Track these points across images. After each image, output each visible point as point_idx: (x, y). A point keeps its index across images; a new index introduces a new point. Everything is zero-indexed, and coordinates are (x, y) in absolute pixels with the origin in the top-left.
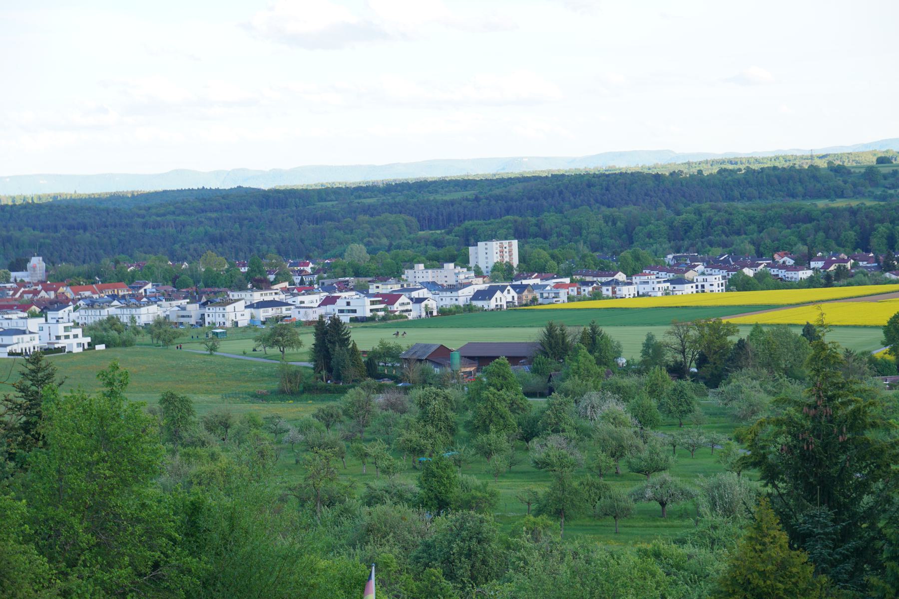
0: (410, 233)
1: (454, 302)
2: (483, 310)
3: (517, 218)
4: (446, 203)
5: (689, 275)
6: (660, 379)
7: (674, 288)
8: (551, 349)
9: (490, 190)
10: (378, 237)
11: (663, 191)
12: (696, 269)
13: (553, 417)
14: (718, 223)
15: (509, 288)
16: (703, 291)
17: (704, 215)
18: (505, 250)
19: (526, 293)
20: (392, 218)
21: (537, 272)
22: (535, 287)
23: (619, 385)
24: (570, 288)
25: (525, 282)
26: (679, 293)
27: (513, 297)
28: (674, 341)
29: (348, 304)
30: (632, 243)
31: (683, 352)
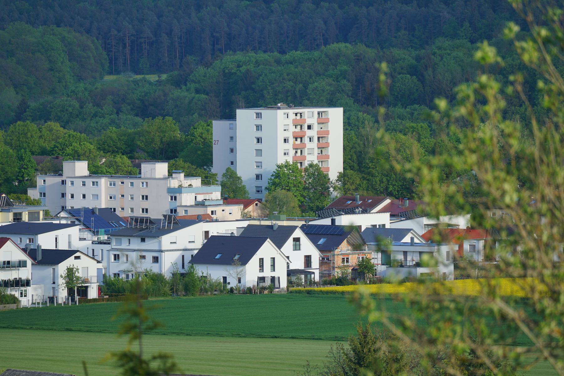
1: (147, 265)
15: (298, 233)
18: (309, 133)
19: (344, 247)
27: (308, 259)
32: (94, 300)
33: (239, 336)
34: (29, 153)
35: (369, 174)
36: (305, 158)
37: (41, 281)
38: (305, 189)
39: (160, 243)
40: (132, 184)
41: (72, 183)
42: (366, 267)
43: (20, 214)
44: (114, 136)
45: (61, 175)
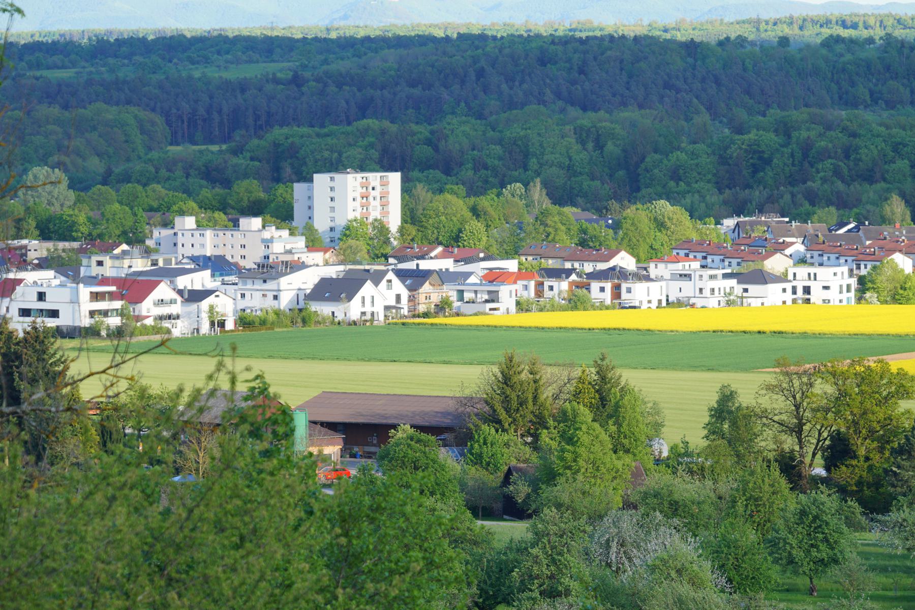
0: (150, 149)
1: (269, 303)
2: (333, 323)
3: (386, 124)
4: (227, 86)
5: (775, 264)
6: (766, 488)
7: (746, 290)
8: (507, 410)
9: (326, 62)
10: (78, 154)
11: (703, 80)
12: (788, 251)
13: (545, 562)
14: (824, 154)
15: (391, 275)
16: (808, 301)
17: (795, 134)
18: (373, 193)
19: (426, 287)
20: (111, 113)
21: (440, 243)
22: (444, 277)
23: (676, 497)
24: (521, 283)
25: (425, 265)
26: (756, 303)
27: (398, 298)
28: (779, 405)
29: (41, 296)
30: (638, 190)
31: (797, 430)
32: (232, 331)
33: (363, 360)
34: (141, 210)
35: (422, 226)
36: (369, 214)
37: (189, 314)
38: (371, 239)
39: (279, 284)
40: (232, 235)
41: (183, 235)
42: (446, 303)
43: (157, 260)
44: (209, 195)
45: (173, 228)
